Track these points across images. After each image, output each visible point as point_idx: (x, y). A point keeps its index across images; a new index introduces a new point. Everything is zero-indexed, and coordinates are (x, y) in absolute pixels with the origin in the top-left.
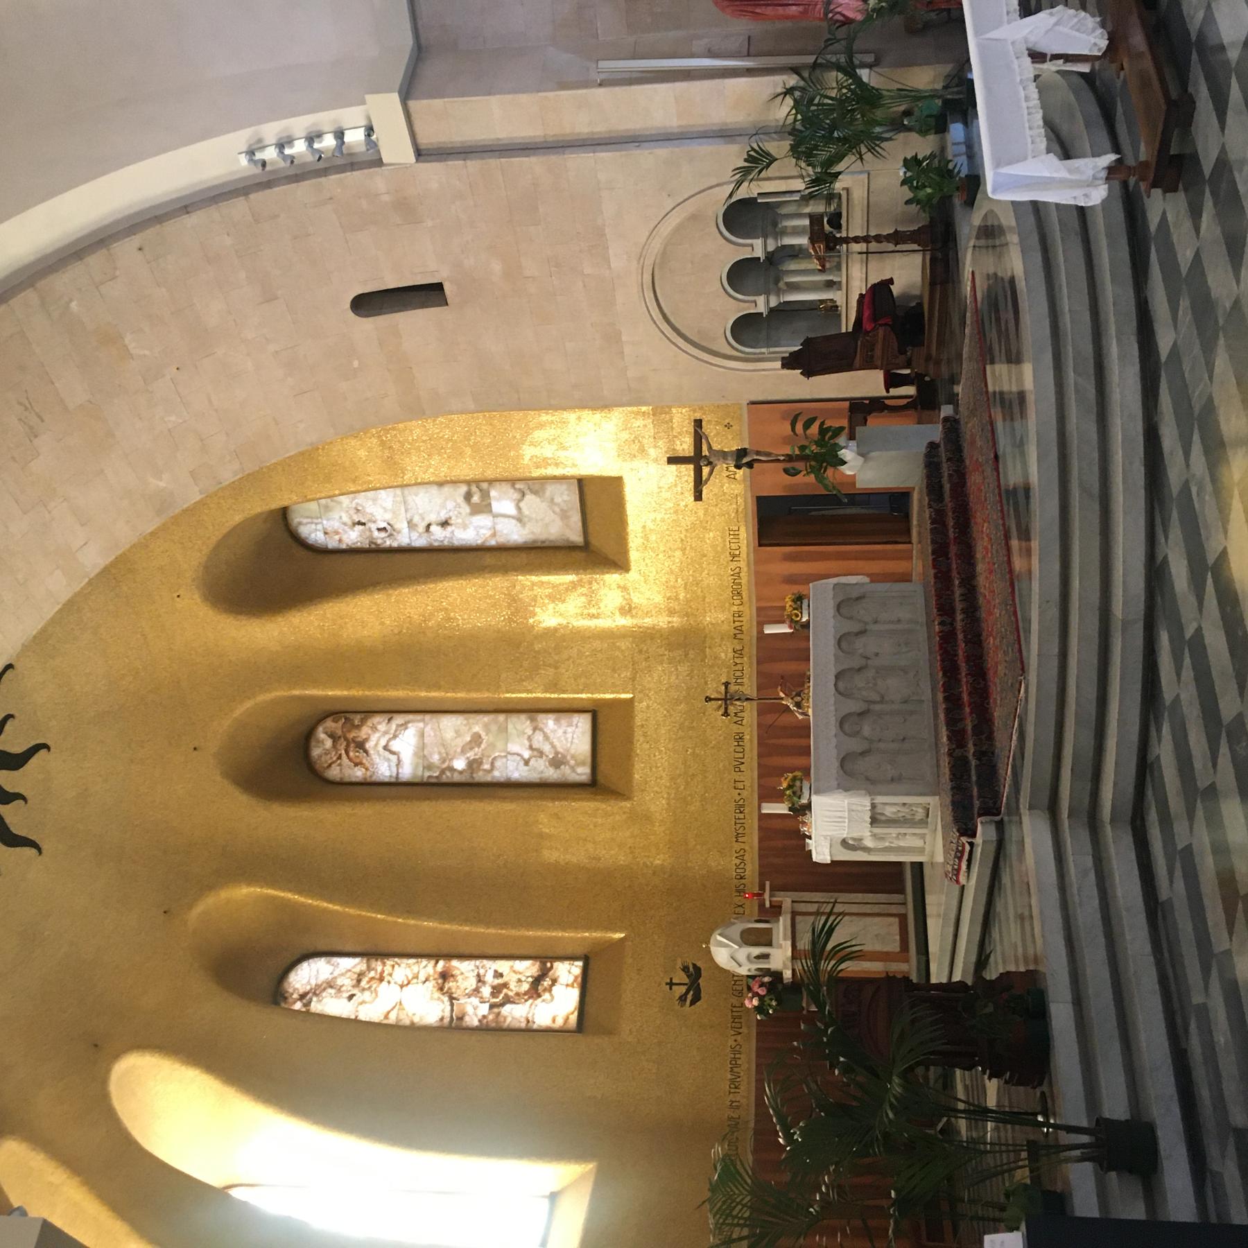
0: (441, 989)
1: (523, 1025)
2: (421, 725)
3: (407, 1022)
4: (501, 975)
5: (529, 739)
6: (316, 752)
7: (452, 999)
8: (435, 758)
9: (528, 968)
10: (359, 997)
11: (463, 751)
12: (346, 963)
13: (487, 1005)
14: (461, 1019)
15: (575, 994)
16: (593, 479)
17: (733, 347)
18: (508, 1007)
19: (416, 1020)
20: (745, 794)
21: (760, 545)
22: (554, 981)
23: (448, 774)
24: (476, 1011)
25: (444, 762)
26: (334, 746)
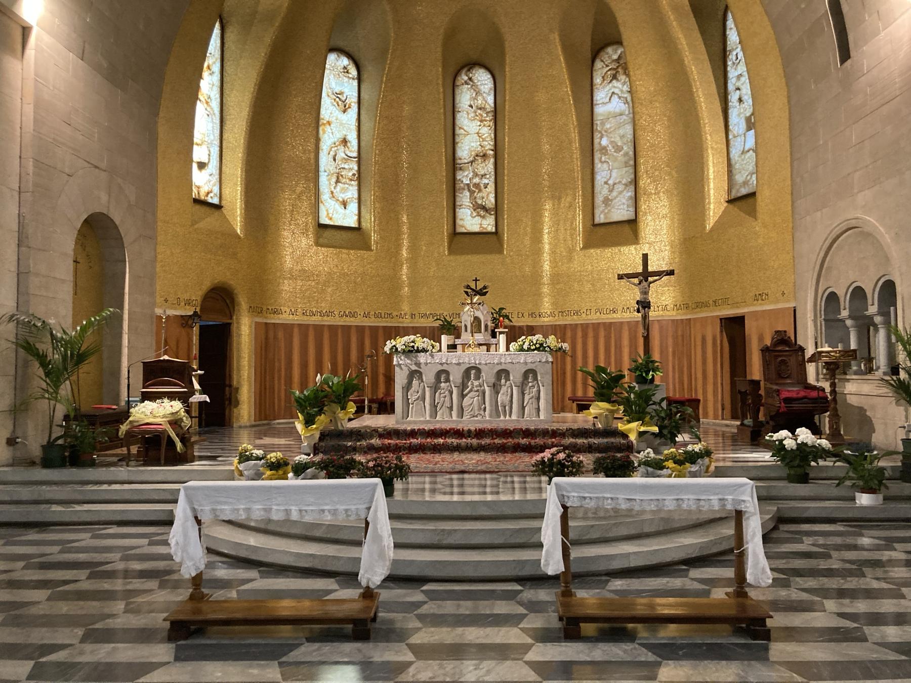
1: (458, 203)
2: (627, 112)
3: (457, 140)
4: (486, 188)
5: (620, 182)
6: (610, 50)
7: (472, 162)
9: (490, 201)
11: (612, 142)
12: (490, 100)
13: (468, 182)
14: (461, 169)
15: (476, 229)
16: (755, 201)
17: (874, 290)
18: (468, 194)
19: (459, 145)
20: (584, 315)
21: (721, 319)
22: (483, 217)
26: (614, 61)
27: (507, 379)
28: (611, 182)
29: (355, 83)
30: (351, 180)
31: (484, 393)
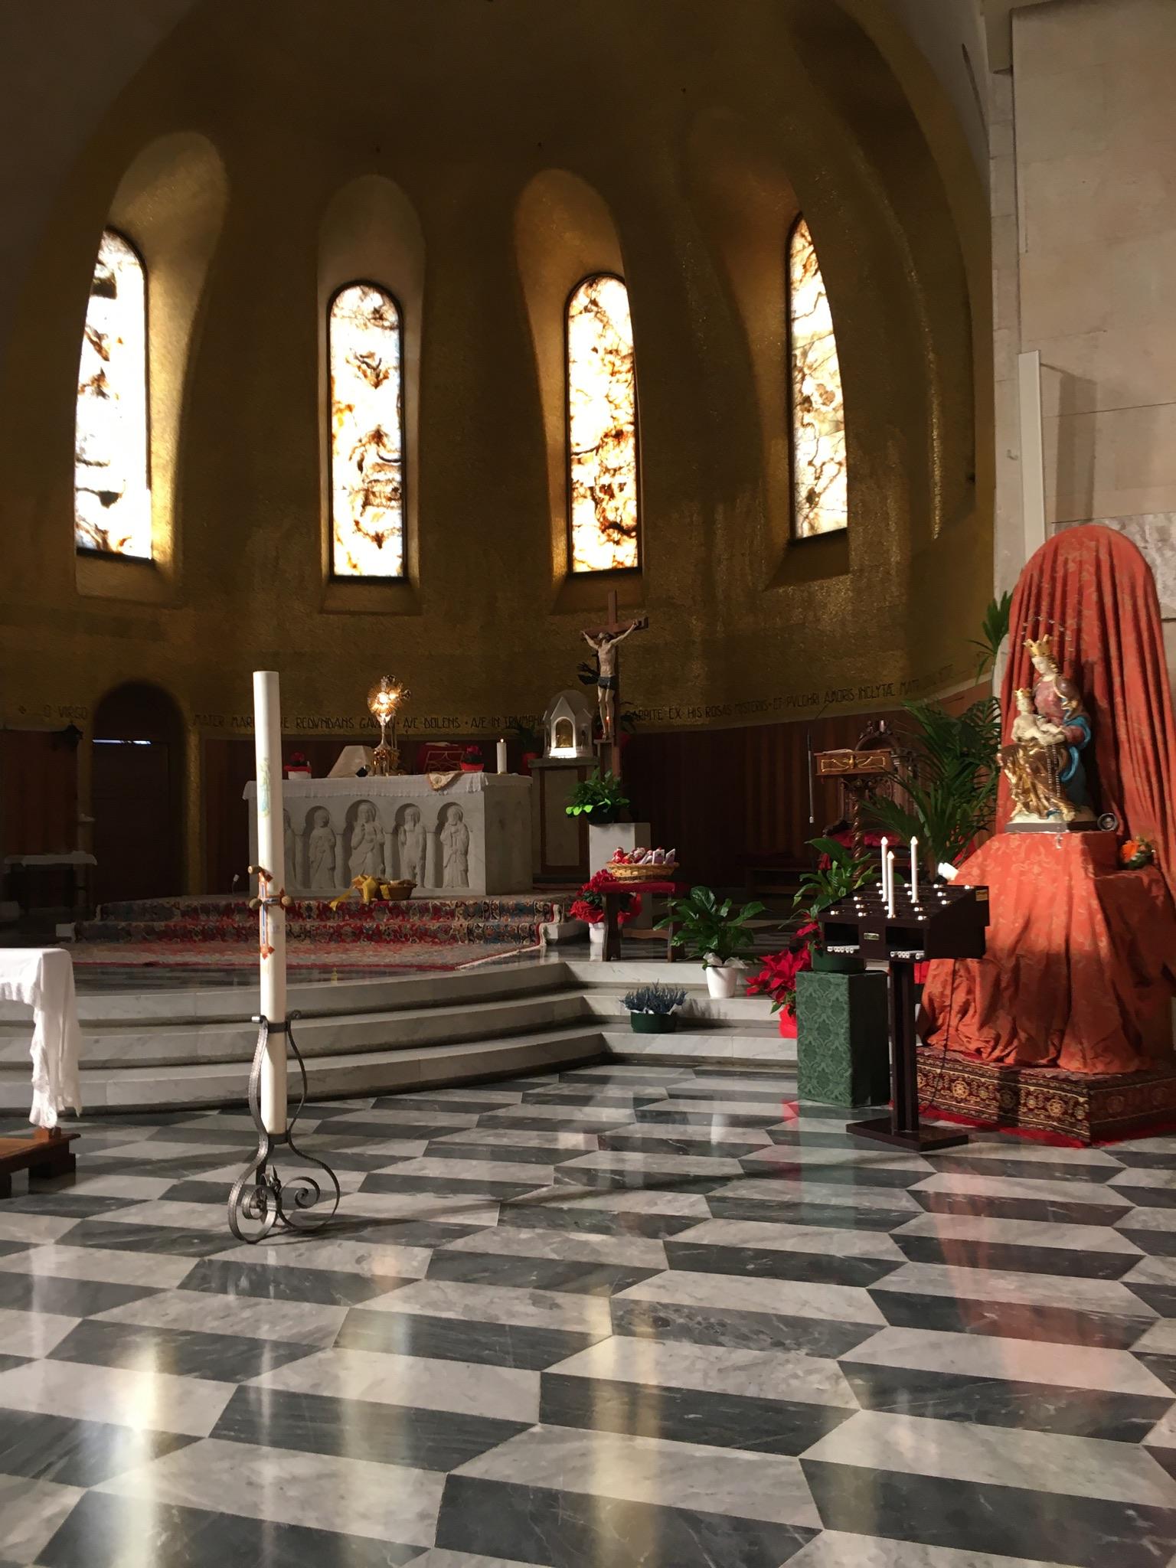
0: (606, 436)
4: (621, 490)
7: (597, 449)
8: (810, 358)
9: (628, 514)
10: (596, 357)
13: (592, 484)
22: (617, 543)
23: (799, 376)
24: (583, 474)
25: (810, 367)
27: (416, 819)
28: (817, 463)
29: (394, 336)
30: (390, 499)
31: (382, 845)
